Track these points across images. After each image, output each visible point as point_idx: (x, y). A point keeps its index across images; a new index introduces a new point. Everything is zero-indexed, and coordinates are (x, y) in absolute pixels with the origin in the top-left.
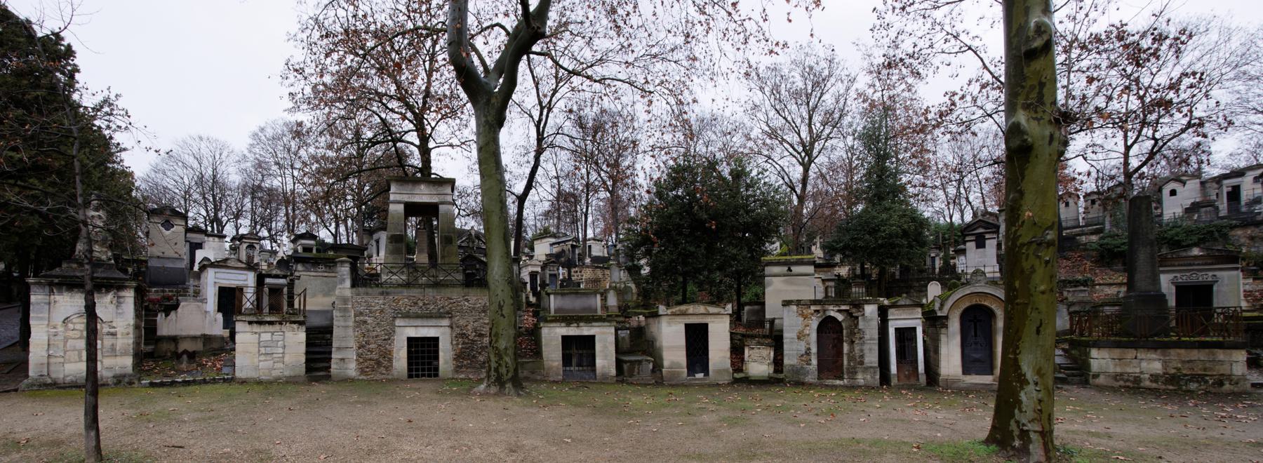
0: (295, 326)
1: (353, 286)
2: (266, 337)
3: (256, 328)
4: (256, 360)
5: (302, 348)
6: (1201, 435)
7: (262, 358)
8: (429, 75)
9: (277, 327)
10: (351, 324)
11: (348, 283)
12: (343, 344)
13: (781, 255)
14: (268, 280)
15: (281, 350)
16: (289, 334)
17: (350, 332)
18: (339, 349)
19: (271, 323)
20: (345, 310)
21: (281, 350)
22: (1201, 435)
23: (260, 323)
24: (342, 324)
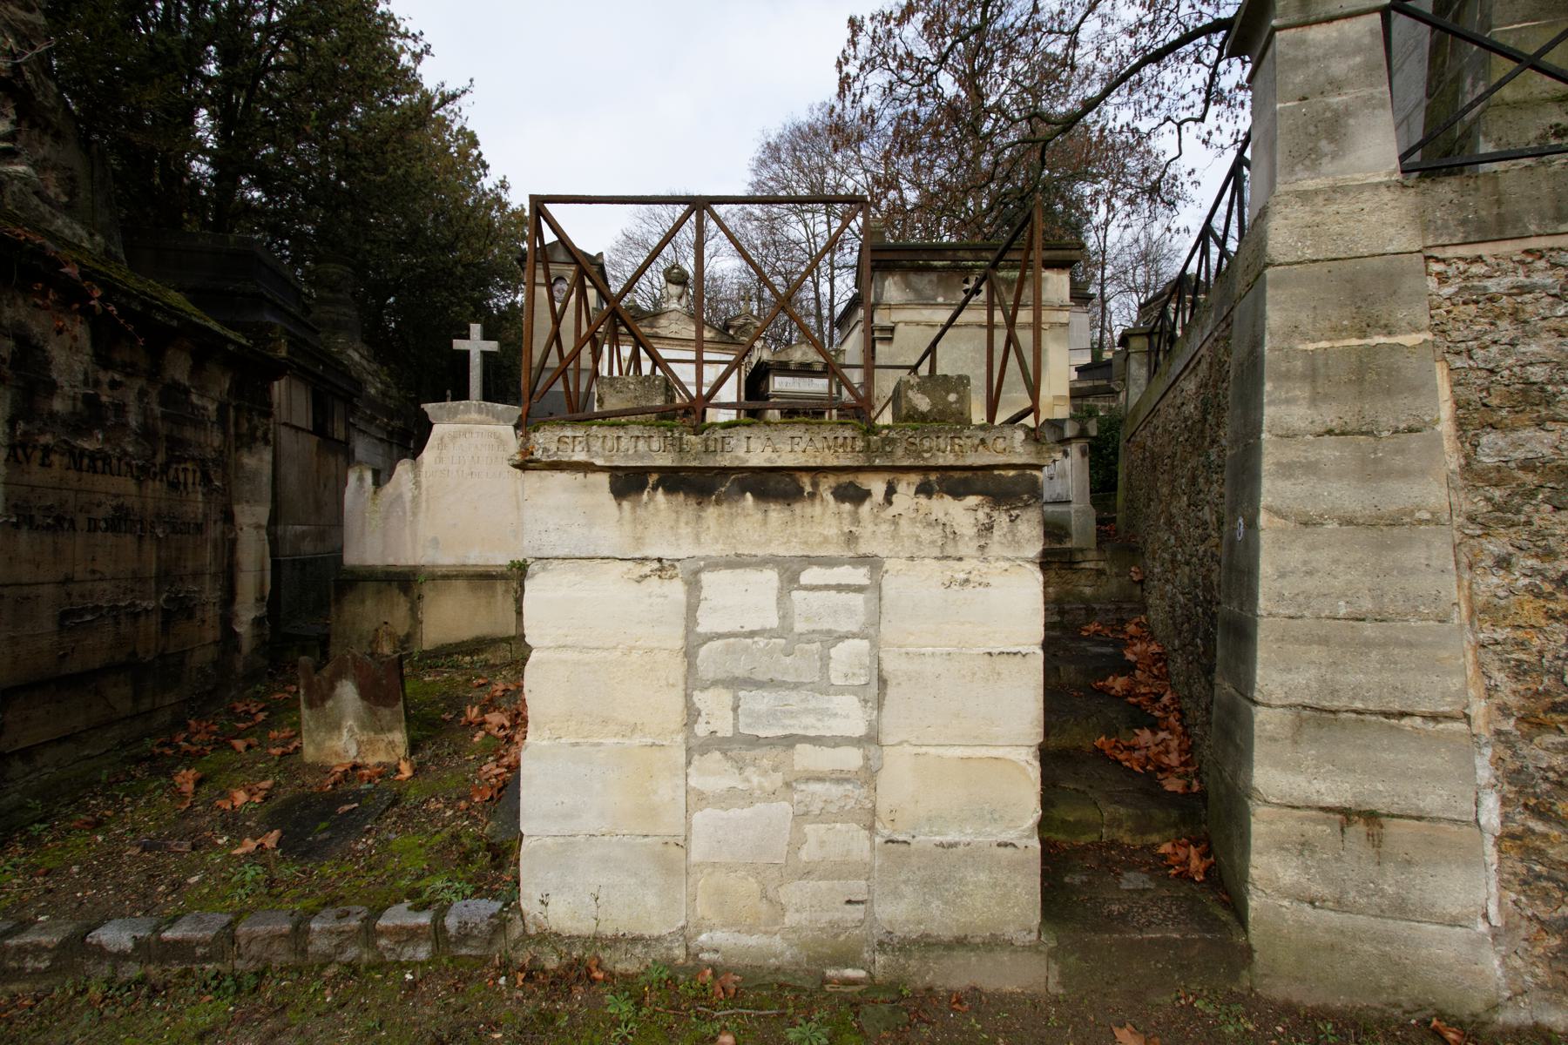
0: (962, 513)
1: (1436, 155)
2: (741, 601)
3: (666, 524)
4: (668, 791)
5: (1018, 707)
6: (48, 243)
7: (713, 775)
8: (832, 280)
9: (823, 520)
10: (1433, 491)
11: (1377, 148)
12: (1363, 682)
13: (225, 433)
14: (779, 384)
15: (849, 716)
16: (914, 583)
17: (1434, 573)
18: (1317, 718)
19: (775, 486)
20: (1371, 375)
21: (849, 716)
22: (48, 243)
23: (697, 484)
24: (1345, 496)
